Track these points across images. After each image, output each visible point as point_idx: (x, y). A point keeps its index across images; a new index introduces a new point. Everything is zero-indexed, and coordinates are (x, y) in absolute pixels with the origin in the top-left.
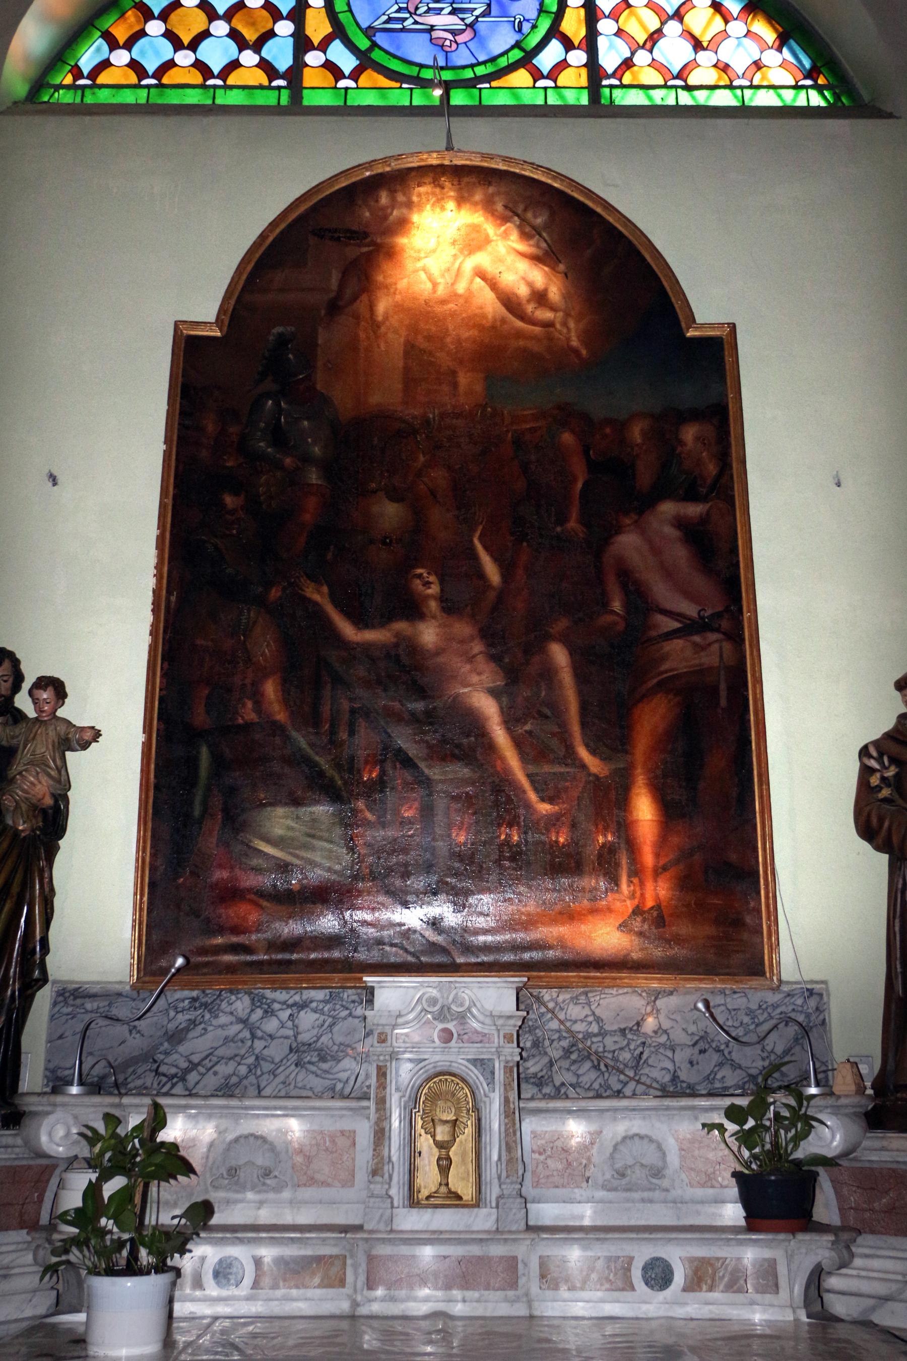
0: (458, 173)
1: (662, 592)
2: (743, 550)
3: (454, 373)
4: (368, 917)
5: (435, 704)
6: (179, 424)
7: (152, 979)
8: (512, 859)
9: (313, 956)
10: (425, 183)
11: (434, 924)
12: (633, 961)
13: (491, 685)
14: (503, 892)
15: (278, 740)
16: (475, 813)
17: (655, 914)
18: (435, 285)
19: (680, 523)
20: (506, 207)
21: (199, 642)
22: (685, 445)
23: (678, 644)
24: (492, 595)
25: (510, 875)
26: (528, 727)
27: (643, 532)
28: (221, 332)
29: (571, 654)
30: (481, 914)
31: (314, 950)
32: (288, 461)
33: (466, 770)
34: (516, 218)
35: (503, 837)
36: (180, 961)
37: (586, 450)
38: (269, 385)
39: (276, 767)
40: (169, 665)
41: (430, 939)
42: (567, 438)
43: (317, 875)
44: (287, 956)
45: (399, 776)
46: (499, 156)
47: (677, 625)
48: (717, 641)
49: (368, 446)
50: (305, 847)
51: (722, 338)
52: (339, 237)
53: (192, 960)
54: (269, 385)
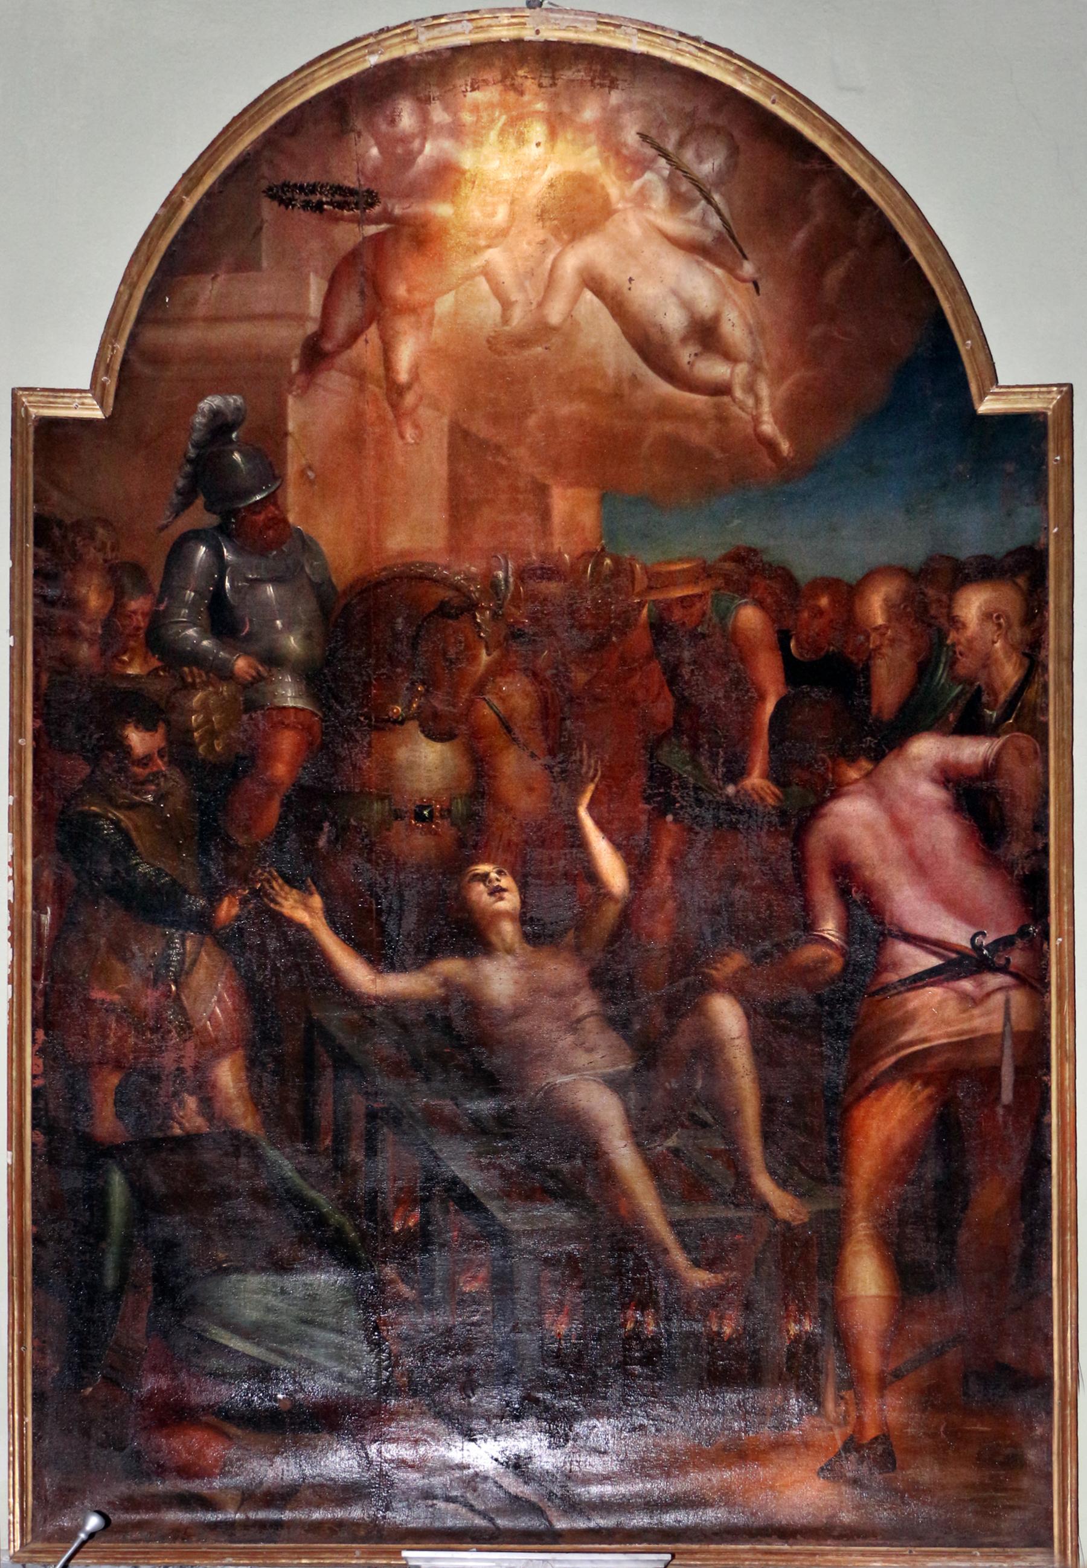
0: (551, 56)
1: (911, 904)
2: (1058, 826)
3: (542, 490)
4: (405, 1452)
5: (513, 1103)
6: (35, 595)
7: (46, 1545)
8: (647, 1361)
9: (317, 1515)
10: (486, 82)
11: (517, 1466)
12: (843, 1526)
13: (611, 1070)
14: (631, 1415)
15: (244, 1163)
16: (582, 1287)
17: (880, 1449)
18: (506, 305)
19: (949, 776)
20: (644, 137)
21: (97, 994)
22: (964, 626)
23: (933, 994)
24: (611, 912)
25: (641, 1387)
26: (672, 1142)
27: (880, 795)
28: (102, 404)
29: (748, 1016)
30: (596, 1451)
31: (318, 1506)
32: (241, 664)
33: (567, 1215)
34: (662, 162)
35: (630, 1326)
36: (93, 1522)
37: (783, 638)
38: (199, 516)
39: (243, 1208)
40: (46, 1034)
41: (513, 1490)
42: (750, 617)
43: (319, 1387)
44: (273, 1515)
45: (454, 1224)
46: (631, 20)
47: (934, 962)
48: (1000, 989)
49: (382, 636)
50: (299, 1339)
51: (1045, 414)
52: (320, 204)
53: (114, 1518)
54: (199, 516)
